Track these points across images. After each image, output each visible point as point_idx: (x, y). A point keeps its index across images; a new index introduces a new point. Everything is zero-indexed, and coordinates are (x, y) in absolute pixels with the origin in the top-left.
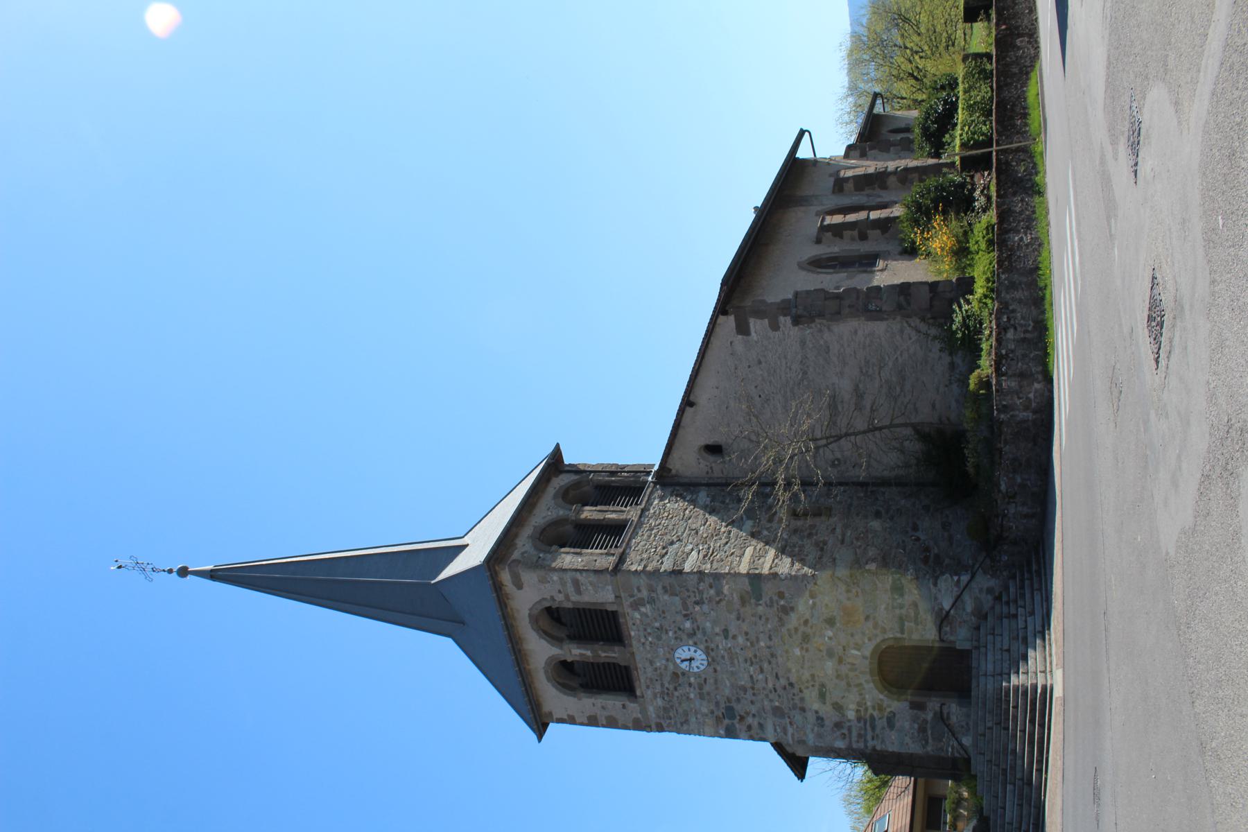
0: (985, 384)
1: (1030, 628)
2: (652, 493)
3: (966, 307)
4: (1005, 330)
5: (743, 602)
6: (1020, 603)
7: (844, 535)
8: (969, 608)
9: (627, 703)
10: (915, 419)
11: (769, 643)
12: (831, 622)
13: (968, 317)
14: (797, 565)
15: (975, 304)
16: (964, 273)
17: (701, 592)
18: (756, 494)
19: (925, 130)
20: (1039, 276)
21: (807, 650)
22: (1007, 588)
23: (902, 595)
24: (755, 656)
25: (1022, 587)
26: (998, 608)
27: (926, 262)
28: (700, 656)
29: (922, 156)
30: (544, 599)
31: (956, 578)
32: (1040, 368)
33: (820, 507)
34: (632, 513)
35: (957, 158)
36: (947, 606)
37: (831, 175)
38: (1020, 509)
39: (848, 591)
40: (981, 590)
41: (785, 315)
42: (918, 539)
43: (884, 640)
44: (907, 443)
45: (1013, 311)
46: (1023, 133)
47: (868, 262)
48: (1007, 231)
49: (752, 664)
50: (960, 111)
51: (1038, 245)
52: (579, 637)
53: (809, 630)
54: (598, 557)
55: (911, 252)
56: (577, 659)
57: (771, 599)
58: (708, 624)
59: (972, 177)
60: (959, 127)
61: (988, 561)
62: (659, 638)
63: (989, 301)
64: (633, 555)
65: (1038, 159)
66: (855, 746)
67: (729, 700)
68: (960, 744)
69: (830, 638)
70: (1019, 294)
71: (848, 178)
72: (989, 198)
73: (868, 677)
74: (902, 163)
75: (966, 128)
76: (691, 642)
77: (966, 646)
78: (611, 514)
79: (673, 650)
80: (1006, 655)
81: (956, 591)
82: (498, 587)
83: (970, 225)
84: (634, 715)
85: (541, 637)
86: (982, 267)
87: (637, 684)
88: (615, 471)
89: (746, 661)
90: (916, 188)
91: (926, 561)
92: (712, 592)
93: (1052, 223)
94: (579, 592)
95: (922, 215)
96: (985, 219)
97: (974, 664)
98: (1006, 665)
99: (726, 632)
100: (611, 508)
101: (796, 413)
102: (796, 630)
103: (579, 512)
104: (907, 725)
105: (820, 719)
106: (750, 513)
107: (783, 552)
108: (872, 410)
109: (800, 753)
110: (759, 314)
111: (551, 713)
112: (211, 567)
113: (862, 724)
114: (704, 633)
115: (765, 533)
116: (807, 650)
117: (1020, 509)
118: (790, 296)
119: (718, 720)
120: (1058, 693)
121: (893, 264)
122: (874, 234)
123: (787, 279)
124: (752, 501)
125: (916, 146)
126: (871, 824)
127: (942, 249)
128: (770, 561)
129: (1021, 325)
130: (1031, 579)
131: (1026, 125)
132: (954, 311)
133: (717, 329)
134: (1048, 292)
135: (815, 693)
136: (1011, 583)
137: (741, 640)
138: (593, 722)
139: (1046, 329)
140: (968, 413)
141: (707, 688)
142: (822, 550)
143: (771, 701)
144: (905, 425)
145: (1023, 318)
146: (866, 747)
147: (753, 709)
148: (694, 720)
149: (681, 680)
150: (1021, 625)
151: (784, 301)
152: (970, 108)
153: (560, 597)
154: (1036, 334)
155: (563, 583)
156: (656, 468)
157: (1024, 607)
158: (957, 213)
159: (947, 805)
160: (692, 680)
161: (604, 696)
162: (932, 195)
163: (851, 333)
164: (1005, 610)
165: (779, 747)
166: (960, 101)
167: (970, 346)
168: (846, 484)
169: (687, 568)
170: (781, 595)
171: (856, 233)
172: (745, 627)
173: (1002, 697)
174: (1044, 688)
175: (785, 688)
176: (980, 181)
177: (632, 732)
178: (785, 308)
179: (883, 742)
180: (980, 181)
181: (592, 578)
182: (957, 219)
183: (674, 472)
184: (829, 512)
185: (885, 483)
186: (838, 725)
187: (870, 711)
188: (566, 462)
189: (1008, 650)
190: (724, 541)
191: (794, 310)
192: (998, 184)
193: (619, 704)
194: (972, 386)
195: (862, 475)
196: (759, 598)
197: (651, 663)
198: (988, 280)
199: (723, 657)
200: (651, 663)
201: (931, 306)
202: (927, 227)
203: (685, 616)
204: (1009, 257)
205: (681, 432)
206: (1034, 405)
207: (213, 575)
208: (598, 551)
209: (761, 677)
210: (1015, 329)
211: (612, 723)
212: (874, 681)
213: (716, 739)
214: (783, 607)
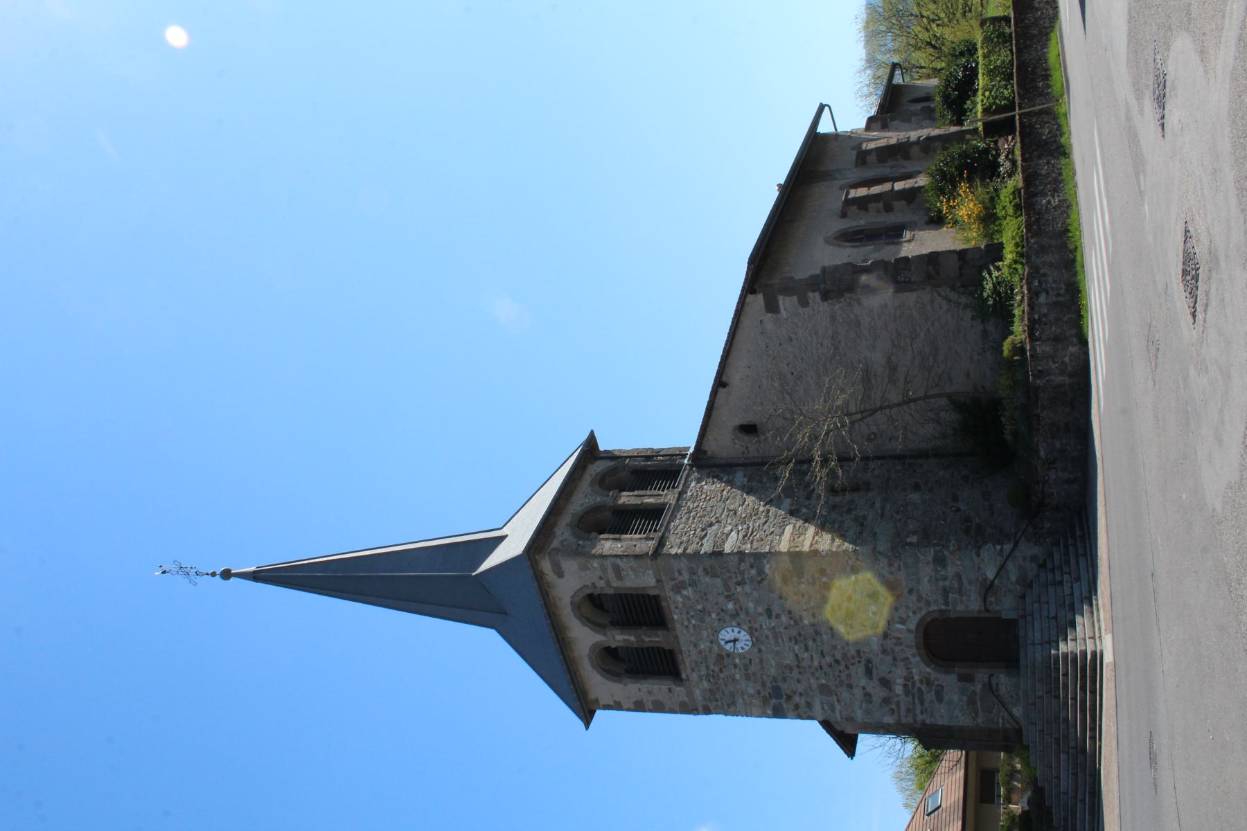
0: (1019, 350)
1: (1077, 593)
3: (995, 274)
4: (1037, 294)
6: (1066, 569)
7: (883, 509)
9: (673, 687)
11: (812, 620)
13: (999, 283)
14: (838, 541)
15: (1005, 271)
16: (992, 239)
17: (742, 573)
18: (793, 472)
21: (851, 627)
22: (1051, 555)
23: (945, 567)
24: (800, 634)
25: (1067, 554)
28: (744, 636)
29: (944, 124)
30: (586, 586)
31: (998, 547)
32: (1074, 332)
33: (854, 490)
35: (980, 124)
36: (990, 575)
37: (853, 148)
39: (890, 565)
40: (1024, 559)
41: (814, 291)
42: (958, 510)
44: (942, 414)
45: (1044, 275)
47: (894, 234)
48: (1035, 195)
49: (796, 642)
50: (980, 76)
51: (1067, 207)
52: (624, 623)
55: (937, 221)
56: (621, 644)
59: (996, 142)
60: (980, 92)
62: (702, 621)
63: (1019, 267)
65: (1062, 121)
66: (904, 721)
67: (775, 679)
68: (1011, 714)
69: (874, 613)
70: (1049, 258)
72: (1014, 163)
73: (914, 651)
75: (987, 94)
77: (1012, 615)
78: (649, 499)
79: (717, 632)
82: (539, 576)
83: (996, 190)
85: (584, 624)
86: (1010, 233)
87: (682, 667)
88: (650, 455)
89: (790, 639)
91: (967, 531)
92: (753, 572)
94: (619, 577)
95: (947, 184)
96: (1011, 184)
97: (1021, 634)
98: (1053, 632)
99: (769, 612)
100: (648, 492)
101: (829, 388)
103: (616, 498)
104: (956, 698)
105: (867, 696)
106: (788, 491)
108: (906, 383)
109: (849, 730)
110: (788, 290)
111: (597, 700)
113: (910, 699)
114: (747, 614)
115: (804, 510)
116: (851, 627)
119: (765, 701)
120: (1108, 658)
123: (819, 253)
124: (789, 479)
127: (969, 216)
129: (1053, 289)
131: (1049, 86)
132: (984, 278)
133: (747, 308)
135: (861, 669)
137: (784, 618)
138: (639, 707)
139: (1079, 291)
141: (752, 669)
142: (862, 524)
144: (940, 395)
145: (1055, 282)
147: (800, 688)
148: (740, 701)
149: (726, 661)
152: (991, 73)
153: (601, 584)
155: (603, 568)
156: (691, 450)
157: (1069, 573)
158: (983, 180)
159: (1000, 777)
160: (737, 661)
161: (651, 681)
162: (956, 162)
164: (1050, 576)
165: (827, 725)
167: (1001, 311)
169: (727, 548)
171: (881, 205)
173: (1051, 666)
174: (1094, 654)
175: (830, 665)
176: (1004, 146)
178: (814, 283)
180: (1004, 146)
181: (633, 563)
183: (709, 453)
184: (867, 487)
185: (921, 455)
186: (886, 701)
187: (918, 684)
188: (602, 448)
189: (1055, 618)
190: (763, 520)
191: (823, 286)
192: (1022, 148)
193: (665, 688)
194: (1006, 353)
195: (898, 447)
197: (695, 645)
198: (1017, 245)
199: (767, 637)
200: (695, 645)
201: (961, 275)
202: (953, 195)
203: (727, 597)
204: (1038, 220)
205: (715, 413)
206: (1069, 369)
207: (256, 576)
208: (637, 536)
209: (806, 655)
210: (1047, 293)
211: (659, 708)
212: (920, 655)
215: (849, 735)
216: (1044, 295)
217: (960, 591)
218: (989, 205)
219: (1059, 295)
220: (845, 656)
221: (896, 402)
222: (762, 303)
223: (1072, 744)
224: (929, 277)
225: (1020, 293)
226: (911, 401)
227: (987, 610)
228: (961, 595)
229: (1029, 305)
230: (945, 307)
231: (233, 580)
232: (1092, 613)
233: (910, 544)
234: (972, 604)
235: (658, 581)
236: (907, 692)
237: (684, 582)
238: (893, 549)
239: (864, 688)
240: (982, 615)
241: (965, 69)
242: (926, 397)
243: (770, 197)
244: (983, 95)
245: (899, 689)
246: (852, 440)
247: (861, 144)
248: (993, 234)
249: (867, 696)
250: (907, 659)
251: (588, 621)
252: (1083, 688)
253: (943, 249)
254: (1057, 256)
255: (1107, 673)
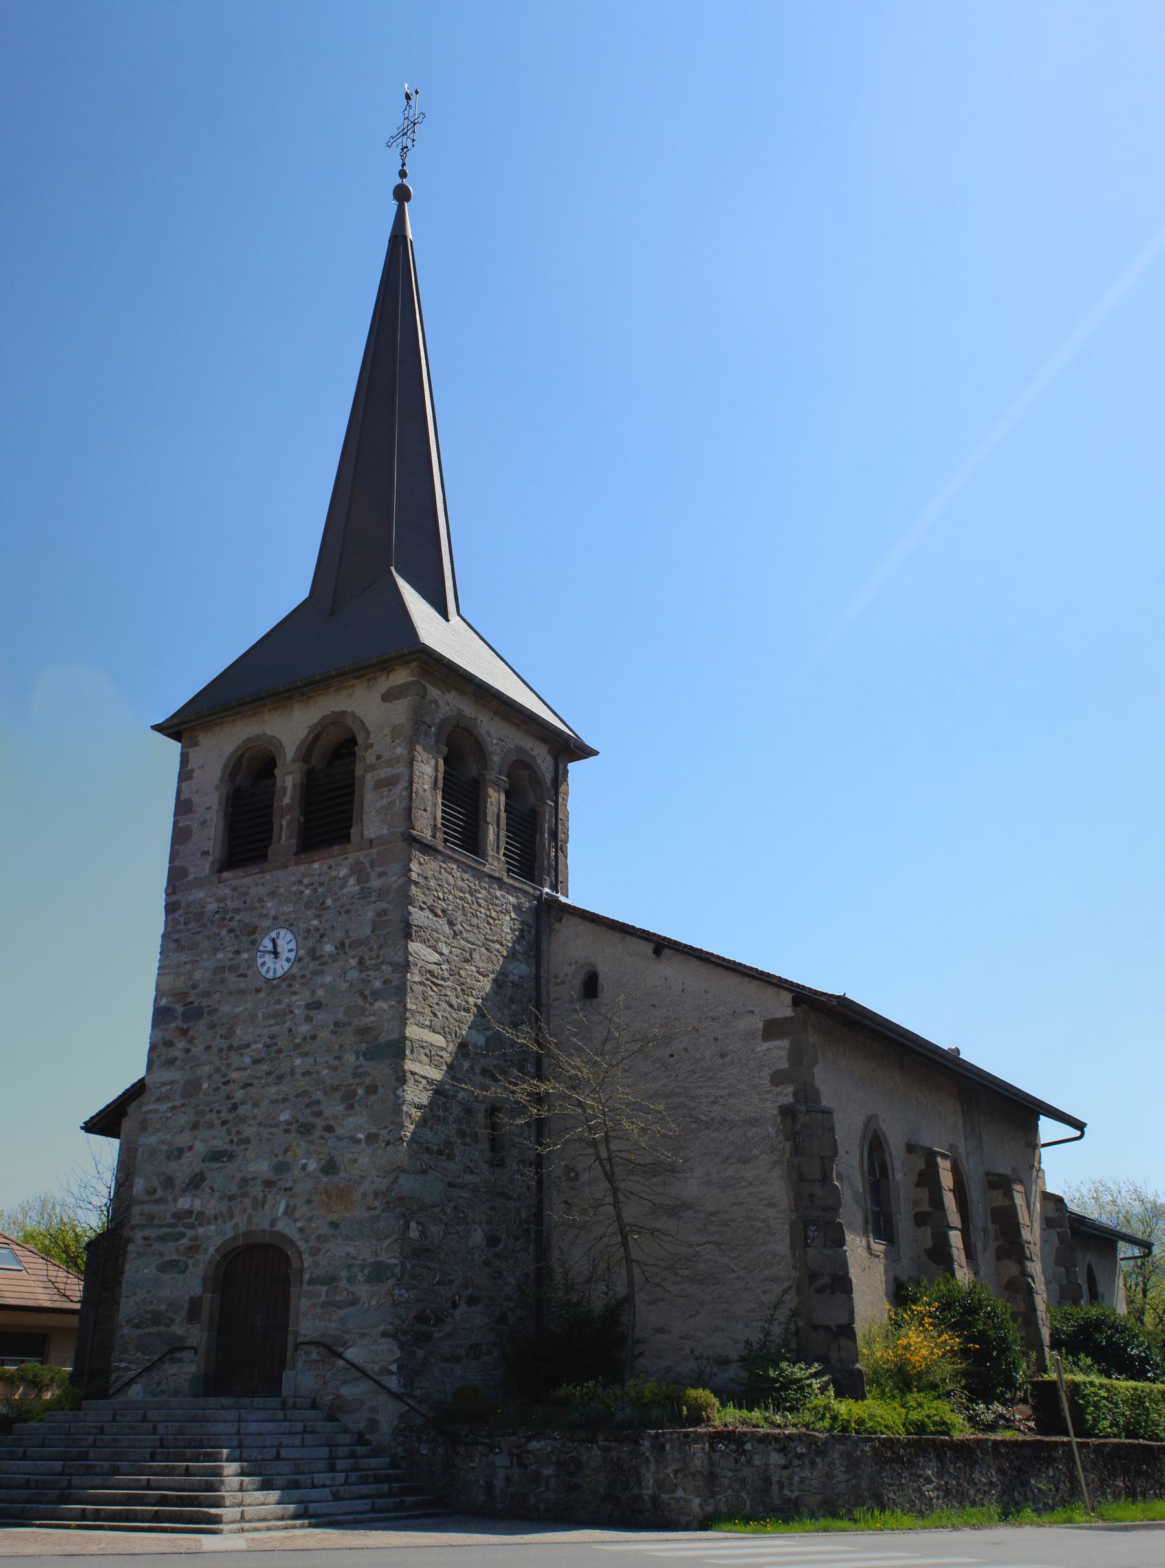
0: (697, 1416)
1: (313, 1494)
2: (525, 893)
3: (816, 1384)
4: (783, 1450)
5: (362, 1032)
6: (353, 1476)
7: (462, 1186)
8: (350, 1391)
9: (211, 859)
10: (638, 1298)
11: (299, 1071)
12: (330, 1167)
13: (801, 1388)
14: (416, 1114)
15: (820, 1401)
16: (871, 1382)
17: (377, 967)
18: (524, 1050)
19: (1096, 1325)
20: (871, 1509)
21: (286, 1131)
22: (376, 1454)
23: (369, 1280)
24: (279, 1051)
25: (378, 1480)
26: (347, 1439)
27: (885, 1321)
28: (281, 967)
29: (1053, 1318)
30: (368, 733)
31: (394, 1368)
32: (724, 1509)
33: (502, 1135)
34: (495, 864)
35: (1054, 1376)
36: (351, 1354)
37: (1014, 1169)
38: (502, 1473)
39: (376, 1194)
40: (374, 1410)
41: (795, 1095)
42: (455, 1306)
43: (299, 1253)
44: (602, 1287)
45: (813, 1464)
46: (1101, 1489)
47: (882, 1226)
48: (940, 1458)
49: (268, 1046)
50: (1132, 1383)
51: (921, 1511)
52: (311, 786)
53: (317, 1133)
54: (429, 814)
55: (900, 1296)
56: (279, 784)
57: (367, 1074)
58: (328, 979)
59: (1024, 1401)
60: (1105, 1381)
61: (419, 1421)
62: (308, 906)
63: (827, 1423)
64: (434, 865)
65: (1060, 1513)
66: (135, 1210)
67: (213, 1012)
68: (132, 1381)
69: (304, 1167)
70: (840, 1474)
71: (1012, 1198)
72: (992, 1427)
73: (243, 1228)
74: (1039, 1285)
75: (1103, 1393)
76: (302, 953)
77: (287, 1389)
78: (494, 834)
79: (290, 927)
80: (270, 1453)
81: (373, 1368)
82: (386, 665)
83: (948, 1394)
84: (191, 869)
85: (311, 729)
86: (879, 1412)
87: (240, 872)
88: (558, 839)
89: (272, 1037)
90: (1001, 1306)
91: (422, 1318)
92: (378, 984)
93: (956, 1535)
94: (379, 785)
95: (959, 1315)
96: (958, 1419)
97: (258, 1401)
98: (255, 1454)
99: (317, 1005)
100: (503, 833)
101: (648, 1111)
102: (318, 1114)
103: (497, 785)
104: (165, 1293)
105: (180, 1153)
106: (495, 1041)
107: (437, 1092)
108: (652, 1231)
109: (127, 1124)
110: (796, 1054)
111: (196, 744)
112: (410, 236)
113: (169, 1220)
114: (315, 973)
115: (466, 1065)
116: (286, 1131)
117: (502, 1473)
118: (824, 1103)
119: (181, 996)
120: (208, 1542)
121: (879, 1266)
122: (926, 1237)
123: (851, 1099)
124: (513, 1044)
125: (1068, 1308)
126: (8, 1242)
127: (906, 1348)
128: (424, 1071)
129: (790, 1478)
130: (390, 1494)
131: (1116, 1497)
132: (809, 1365)
133: (771, 991)
134: (844, 1524)
135: (219, 1145)
136: (385, 1460)
137: (305, 1028)
138: (183, 807)
139: (786, 1520)
140: (650, 1388)
141: (231, 978)
142: (440, 1153)
143: (210, 1077)
144: (631, 1284)
145: (803, 1481)
146: (133, 1228)
147: (197, 1050)
148: (183, 958)
149: (245, 938)
150: (319, 1478)
151: (817, 1091)
152: (1137, 1401)
153: (370, 758)
154: (778, 1502)
155: (392, 762)
156: (563, 899)
157: (346, 1483)
158: (965, 1374)
159: (32, 1365)
160: (245, 956)
161: (221, 824)
162: (991, 1333)
163: (767, 1191)
164: (344, 1451)
165: (137, 1091)
166: (1147, 1384)
167: (755, 1392)
168: (540, 1190)
169: (415, 947)
170: (372, 1090)
171: (926, 1207)
172: (324, 1034)
173: (203, 1448)
174: (217, 1520)
175: (229, 1097)
176: (1019, 1413)
177: (167, 866)
178: (807, 1095)
179: (141, 1255)
180: (1019, 1413)
181: (399, 805)
182: (956, 1373)
183: (557, 926)
184: (497, 1163)
185: (542, 1251)
186: (169, 1182)
187: (190, 1233)
188: (571, 766)
189: (278, 1457)
190: (454, 1002)
191: (803, 1108)
192: (1015, 1443)
193: (209, 845)
194: (692, 1393)
195: (555, 1214)
196: (369, 1055)
197: (272, 894)
198: (860, 1422)
199: (279, 1002)
200: (272, 894)
201: (816, 1328)
202: (941, 1323)
203: (342, 944)
204: (899, 1459)
205: (617, 936)
206: (665, 1497)
207: (398, 241)
208: (439, 814)
209: (247, 1060)
210: (785, 1467)
211: (180, 836)
212: (235, 1237)
213: (154, 993)
214: (355, 1092)
215: (119, 1124)
216: (782, 1461)
217: (330, 1304)
218: (924, 1381)
219: (781, 1488)
220: (242, 1120)
221: (624, 1215)
222: (779, 1015)
223: (76, 1480)
224: (813, 1276)
225: (786, 1423)
226: (625, 1237)
227: (297, 1347)
228: (324, 1305)
229: (767, 1435)
230: (765, 1299)
231: (394, 204)
232: (282, 1518)
233: (407, 1227)
234: (308, 1320)
235: (371, 841)
236: (178, 1215)
237: (368, 880)
238: (401, 1199)
239: (190, 1148)
240: (290, 1338)
241: (1145, 1360)
242: (629, 1260)
243: (940, 1036)
244: (1101, 1386)
245: (184, 1203)
246: (567, 1142)
247: (1022, 1183)
248: (879, 1384)
249: (180, 1153)
250: (232, 1217)
251: (315, 737)
252: (164, 1500)
253: (856, 1303)
254: (842, 1486)
255: (184, 1541)
